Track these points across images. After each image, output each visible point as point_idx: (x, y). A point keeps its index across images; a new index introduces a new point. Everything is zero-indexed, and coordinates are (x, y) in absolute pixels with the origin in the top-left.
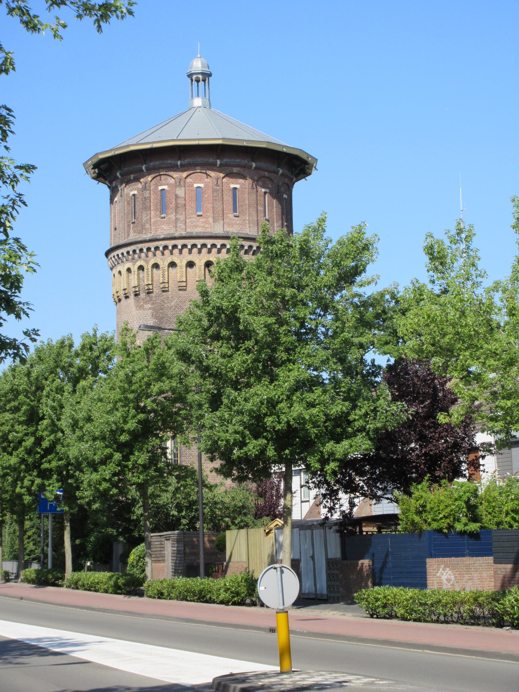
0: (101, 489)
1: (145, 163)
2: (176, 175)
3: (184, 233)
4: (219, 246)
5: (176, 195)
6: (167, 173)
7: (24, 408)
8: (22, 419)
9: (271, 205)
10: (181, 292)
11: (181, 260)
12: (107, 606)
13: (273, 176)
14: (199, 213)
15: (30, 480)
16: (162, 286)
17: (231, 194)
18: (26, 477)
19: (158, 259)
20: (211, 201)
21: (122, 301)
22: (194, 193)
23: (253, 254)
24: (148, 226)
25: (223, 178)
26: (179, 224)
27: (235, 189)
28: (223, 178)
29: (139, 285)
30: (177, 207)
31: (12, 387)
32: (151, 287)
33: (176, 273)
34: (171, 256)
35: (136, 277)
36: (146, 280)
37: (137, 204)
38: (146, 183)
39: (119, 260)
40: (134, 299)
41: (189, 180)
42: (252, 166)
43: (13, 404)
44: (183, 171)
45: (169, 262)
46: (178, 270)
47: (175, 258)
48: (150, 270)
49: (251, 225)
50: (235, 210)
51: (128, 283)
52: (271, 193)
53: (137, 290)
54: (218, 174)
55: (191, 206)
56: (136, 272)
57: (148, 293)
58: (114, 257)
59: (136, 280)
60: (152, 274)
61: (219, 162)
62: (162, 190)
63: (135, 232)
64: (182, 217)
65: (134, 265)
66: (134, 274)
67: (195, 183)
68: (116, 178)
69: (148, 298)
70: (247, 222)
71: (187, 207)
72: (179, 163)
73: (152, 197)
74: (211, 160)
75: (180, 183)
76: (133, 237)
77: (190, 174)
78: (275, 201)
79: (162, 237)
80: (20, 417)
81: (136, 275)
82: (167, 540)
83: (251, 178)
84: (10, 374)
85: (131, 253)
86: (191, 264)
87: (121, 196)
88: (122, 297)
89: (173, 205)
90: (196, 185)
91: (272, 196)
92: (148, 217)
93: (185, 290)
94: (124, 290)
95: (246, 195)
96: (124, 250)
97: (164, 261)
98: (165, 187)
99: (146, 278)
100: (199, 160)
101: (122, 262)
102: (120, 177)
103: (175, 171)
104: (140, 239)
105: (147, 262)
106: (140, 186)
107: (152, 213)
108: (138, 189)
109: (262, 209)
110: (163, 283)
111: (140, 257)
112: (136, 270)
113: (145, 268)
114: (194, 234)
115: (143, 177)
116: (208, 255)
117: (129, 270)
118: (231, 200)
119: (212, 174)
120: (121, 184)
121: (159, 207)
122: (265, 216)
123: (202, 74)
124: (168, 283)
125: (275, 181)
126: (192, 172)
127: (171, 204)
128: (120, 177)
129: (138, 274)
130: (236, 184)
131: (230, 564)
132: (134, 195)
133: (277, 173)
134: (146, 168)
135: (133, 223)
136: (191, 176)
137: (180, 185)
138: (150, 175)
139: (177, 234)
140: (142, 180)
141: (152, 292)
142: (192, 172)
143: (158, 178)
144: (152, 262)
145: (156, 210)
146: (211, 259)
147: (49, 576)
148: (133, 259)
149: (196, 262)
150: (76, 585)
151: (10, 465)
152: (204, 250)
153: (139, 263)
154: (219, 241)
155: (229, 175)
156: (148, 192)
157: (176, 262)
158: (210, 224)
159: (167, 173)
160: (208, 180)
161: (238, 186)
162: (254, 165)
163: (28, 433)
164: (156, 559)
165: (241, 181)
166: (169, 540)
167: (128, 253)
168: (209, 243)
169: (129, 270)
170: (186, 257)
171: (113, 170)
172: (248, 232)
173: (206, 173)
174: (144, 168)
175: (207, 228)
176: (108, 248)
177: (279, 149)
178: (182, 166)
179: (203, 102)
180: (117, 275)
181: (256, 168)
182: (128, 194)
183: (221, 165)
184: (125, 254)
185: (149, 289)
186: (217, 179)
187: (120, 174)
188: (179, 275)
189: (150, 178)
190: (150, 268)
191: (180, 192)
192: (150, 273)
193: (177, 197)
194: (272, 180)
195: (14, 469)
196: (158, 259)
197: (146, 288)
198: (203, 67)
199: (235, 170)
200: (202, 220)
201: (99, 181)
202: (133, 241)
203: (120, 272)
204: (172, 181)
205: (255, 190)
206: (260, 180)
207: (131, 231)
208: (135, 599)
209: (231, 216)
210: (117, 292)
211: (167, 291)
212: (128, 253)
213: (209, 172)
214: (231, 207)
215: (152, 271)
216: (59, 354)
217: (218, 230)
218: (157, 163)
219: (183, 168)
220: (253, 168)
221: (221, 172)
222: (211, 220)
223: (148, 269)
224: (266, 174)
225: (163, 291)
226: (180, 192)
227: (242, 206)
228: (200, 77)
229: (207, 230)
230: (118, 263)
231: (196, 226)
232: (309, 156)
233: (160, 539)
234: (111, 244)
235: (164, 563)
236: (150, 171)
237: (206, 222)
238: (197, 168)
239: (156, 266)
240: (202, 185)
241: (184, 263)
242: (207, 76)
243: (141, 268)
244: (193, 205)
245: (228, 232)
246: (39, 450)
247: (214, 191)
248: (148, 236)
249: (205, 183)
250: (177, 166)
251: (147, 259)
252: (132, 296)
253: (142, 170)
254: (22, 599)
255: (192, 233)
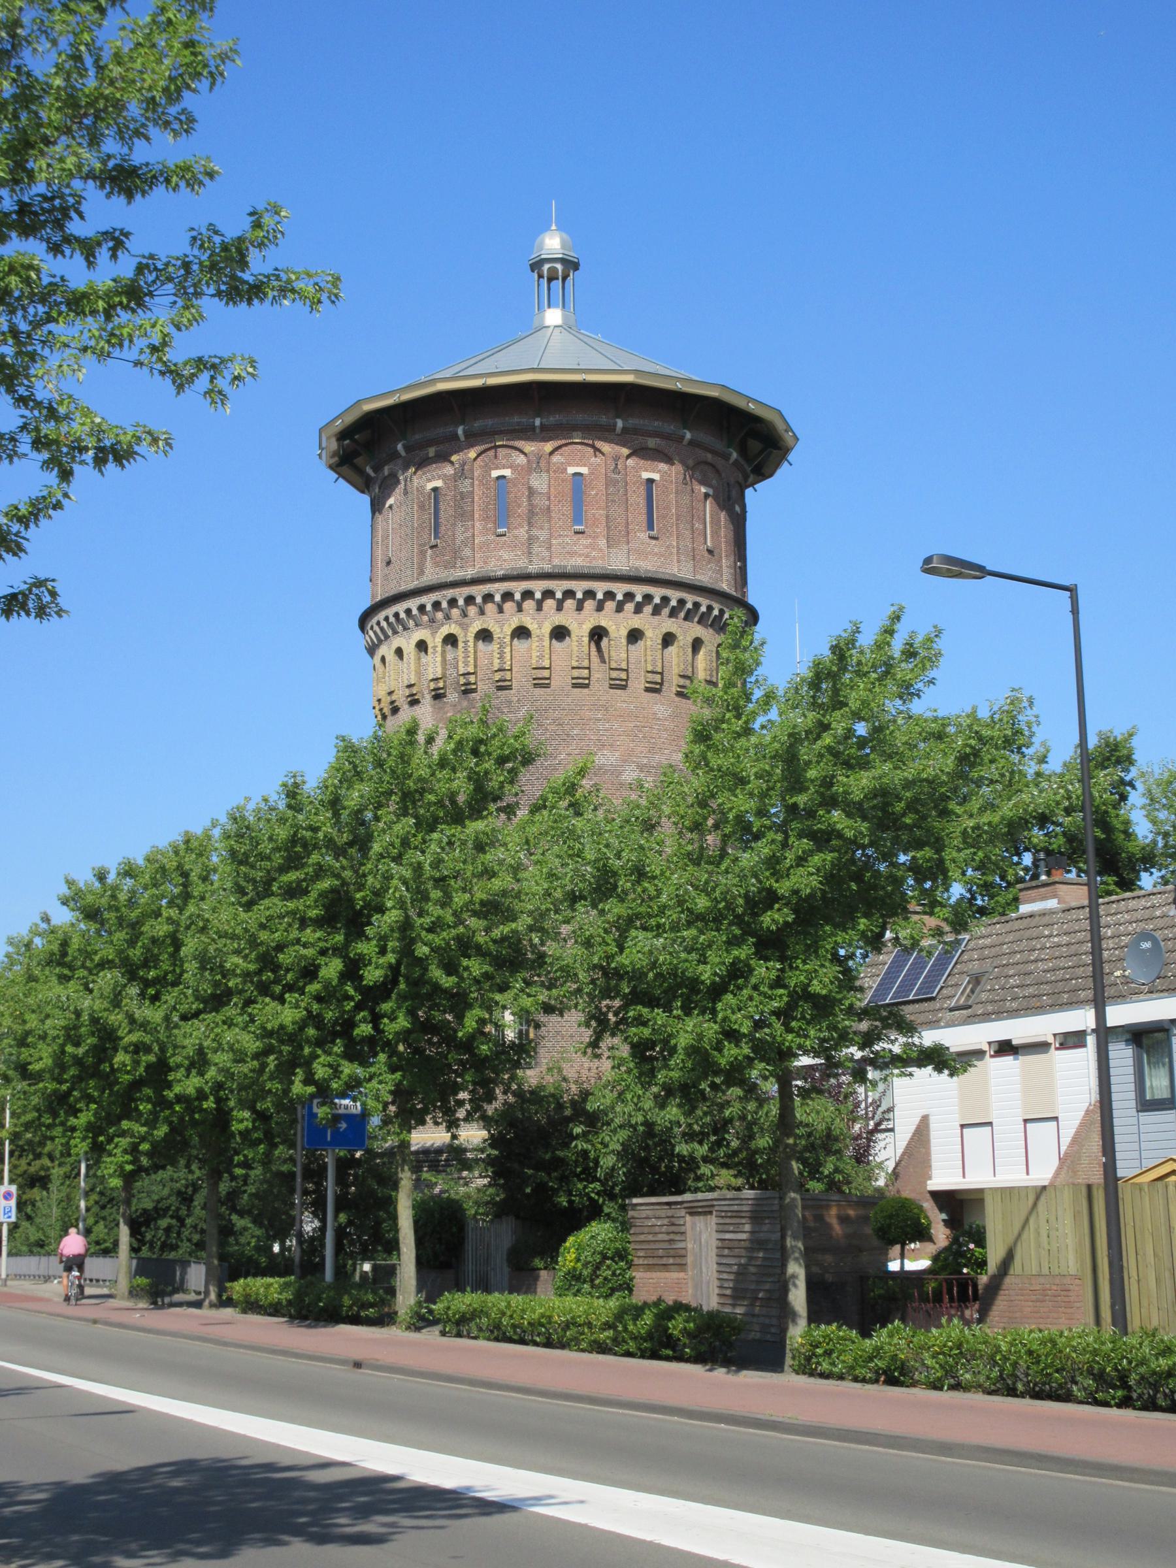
0: (723, 1062)
1: (463, 423)
2: (530, 447)
3: (547, 568)
4: (620, 597)
5: (530, 488)
6: (511, 443)
7: (326, 884)
8: (313, 913)
9: (715, 522)
10: (539, 691)
11: (541, 624)
12: (523, 1377)
13: (719, 462)
14: (577, 528)
15: (330, 1066)
16: (497, 676)
17: (642, 491)
18: (318, 1057)
19: (490, 620)
20: (603, 504)
21: (401, 712)
22: (568, 488)
23: (685, 619)
24: (467, 552)
25: (628, 457)
26: (536, 549)
27: (650, 481)
28: (628, 457)
29: (444, 677)
30: (531, 513)
31: (295, 834)
32: (472, 679)
33: (530, 649)
34: (519, 615)
35: (439, 659)
36: (461, 665)
37: (442, 506)
38: (463, 464)
39: (399, 624)
40: (433, 706)
41: (556, 458)
42: (683, 437)
43: (292, 876)
44: (546, 440)
45: (514, 626)
46: (533, 643)
47: (528, 619)
48: (471, 644)
49: (682, 558)
50: (650, 526)
51: (419, 674)
52: (716, 498)
53: (441, 685)
54: (617, 448)
55: (562, 510)
56: (439, 649)
57: (465, 692)
58: (378, 623)
59: (439, 664)
60: (475, 652)
61: (620, 424)
62: (499, 478)
63: (436, 564)
64: (542, 535)
65: (434, 634)
66: (435, 652)
67: (570, 465)
68: (395, 455)
69: (465, 704)
70: (675, 551)
71: (553, 515)
72: (538, 422)
73: (478, 492)
74: (604, 420)
75: (537, 464)
76: (432, 575)
77: (560, 447)
78: (723, 515)
79: (500, 573)
80: (309, 907)
81: (439, 655)
82: (691, 1214)
83: (683, 463)
84: (183, 846)
85: (429, 608)
86: (560, 633)
87: (406, 493)
88: (402, 702)
89: (523, 510)
90: (571, 470)
91: (719, 505)
92: (469, 534)
93: (547, 686)
94: (410, 686)
95: (673, 496)
96: (413, 604)
97: (502, 625)
98: (507, 472)
99: (463, 659)
100: (580, 417)
101: (405, 629)
102: (403, 453)
103: (528, 439)
104: (451, 579)
105: (465, 627)
106: (449, 470)
107: (477, 524)
108: (444, 478)
109: (701, 527)
110: (499, 670)
111: (448, 617)
112: (440, 645)
113: (461, 640)
114: (569, 570)
115: (456, 452)
116: (596, 614)
117: (422, 646)
118: (642, 502)
119: (606, 447)
120: (406, 468)
121: (491, 513)
122: (705, 543)
123: (562, 261)
124: (511, 670)
125: (723, 475)
126: (564, 442)
127: (519, 506)
128: (403, 453)
129: (444, 653)
130: (653, 472)
131: (1008, 1280)
132: (435, 490)
133: (726, 457)
134: (465, 432)
135: (432, 547)
136: (560, 451)
137: (538, 469)
138: (472, 446)
139: (533, 568)
140: (454, 458)
141: (474, 691)
142: (564, 442)
143: (491, 453)
144: (476, 626)
145: (486, 519)
146: (603, 624)
147: (158, 1284)
148: (432, 621)
149: (573, 626)
150: (421, 1321)
151: (282, 1027)
152: (589, 605)
153: (445, 630)
154: (619, 585)
155: (639, 452)
156: (468, 481)
157: (529, 627)
158: (601, 550)
159: (511, 443)
160: (599, 460)
161: (656, 476)
162: (688, 436)
163: (328, 949)
164: (651, 1261)
165: (663, 466)
166: (711, 1213)
167: (422, 608)
168: (600, 588)
169: (422, 646)
170: (551, 617)
171: (373, 447)
172: (675, 571)
173: (593, 446)
174: (460, 431)
175: (594, 558)
176: (366, 604)
177: (740, 403)
178: (543, 427)
179: (564, 317)
180: (391, 657)
181: (692, 443)
182: (421, 489)
183: (625, 430)
184: (415, 612)
185: (469, 684)
186: (616, 459)
187: (405, 447)
188: (535, 654)
189: (472, 454)
190: (471, 639)
191: (539, 482)
192: (471, 649)
193: (531, 492)
194: (718, 471)
195: (293, 1037)
196: (490, 620)
197: (462, 681)
198: (563, 247)
199: (652, 442)
200: (584, 541)
201: (340, 475)
202: (434, 582)
203: (399, 652)
204: (521, 460)
205: (689, 488)
206: (699, 469)
207: (429, 563)
208: (750, 1377)
209: (643, 535)
210: (390, 693)
211: (509, 688)
212: (422, 608)
213: (598, 444)
214: (643, 518)
215: (475, 646)
216: (404, 759)
217: (619, 562)
218: (490, 422)
219: (546, 433)
220: (685, 442)
221: (624, 446)
222: (602, 543)
223: (466, 642)
224: (709, 456)
225: (500, 688)
226: (539, 482)
227: (664, 517)
228: (559, 266)
229: (594, 564)
230: (395, 632)
231: (572, 554)
232: (789, 428)
233: (670, 1213)
234: (373, 597)
235: (684, 1271)
236: (473, 438)
237: (593, 547)
238: (575, 434)
239: (485, 635)
240: (584, 470)
241: (547, 629)
242: (571, 265)
243: (451, 640)
244: (567, 509)
245: (636, 569)
246: (351, 992)
247: (609, 483)
248: (470, 573)
249: (590, 466)
250: (533, 428)
251: (466, 620)
252: (427, 700)
253: (455, 437)
254: (358, 1365)
255: (565, 567)
